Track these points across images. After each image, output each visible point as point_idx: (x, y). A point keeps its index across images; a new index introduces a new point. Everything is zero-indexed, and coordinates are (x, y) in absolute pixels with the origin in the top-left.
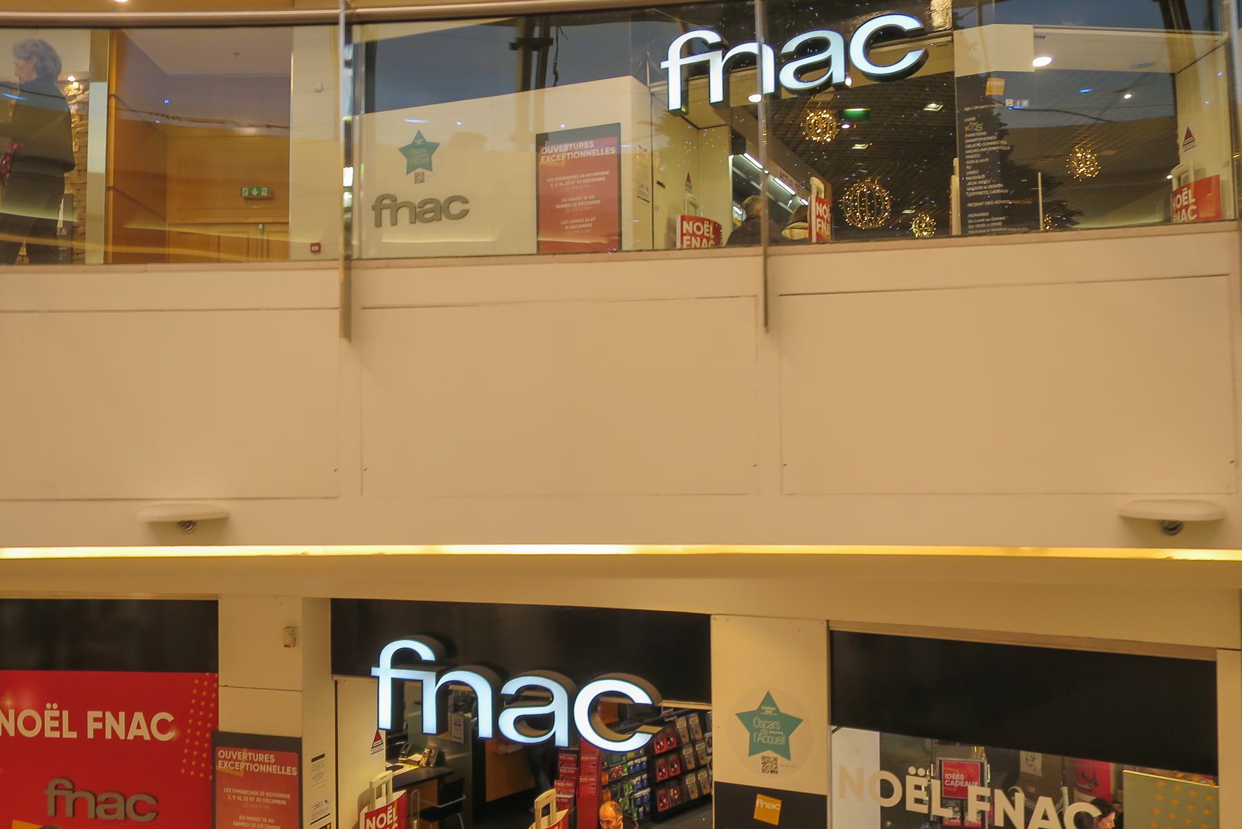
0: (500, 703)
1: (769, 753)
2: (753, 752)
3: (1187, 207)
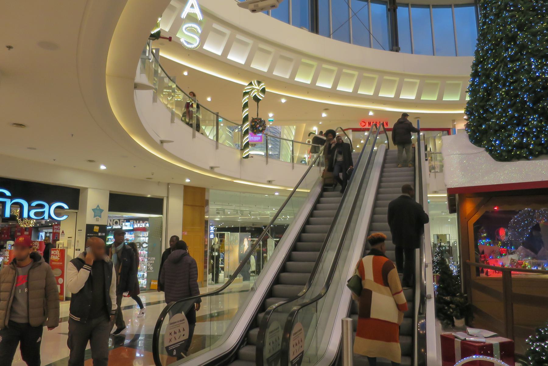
0: (30, 208)
1: (98, 217)
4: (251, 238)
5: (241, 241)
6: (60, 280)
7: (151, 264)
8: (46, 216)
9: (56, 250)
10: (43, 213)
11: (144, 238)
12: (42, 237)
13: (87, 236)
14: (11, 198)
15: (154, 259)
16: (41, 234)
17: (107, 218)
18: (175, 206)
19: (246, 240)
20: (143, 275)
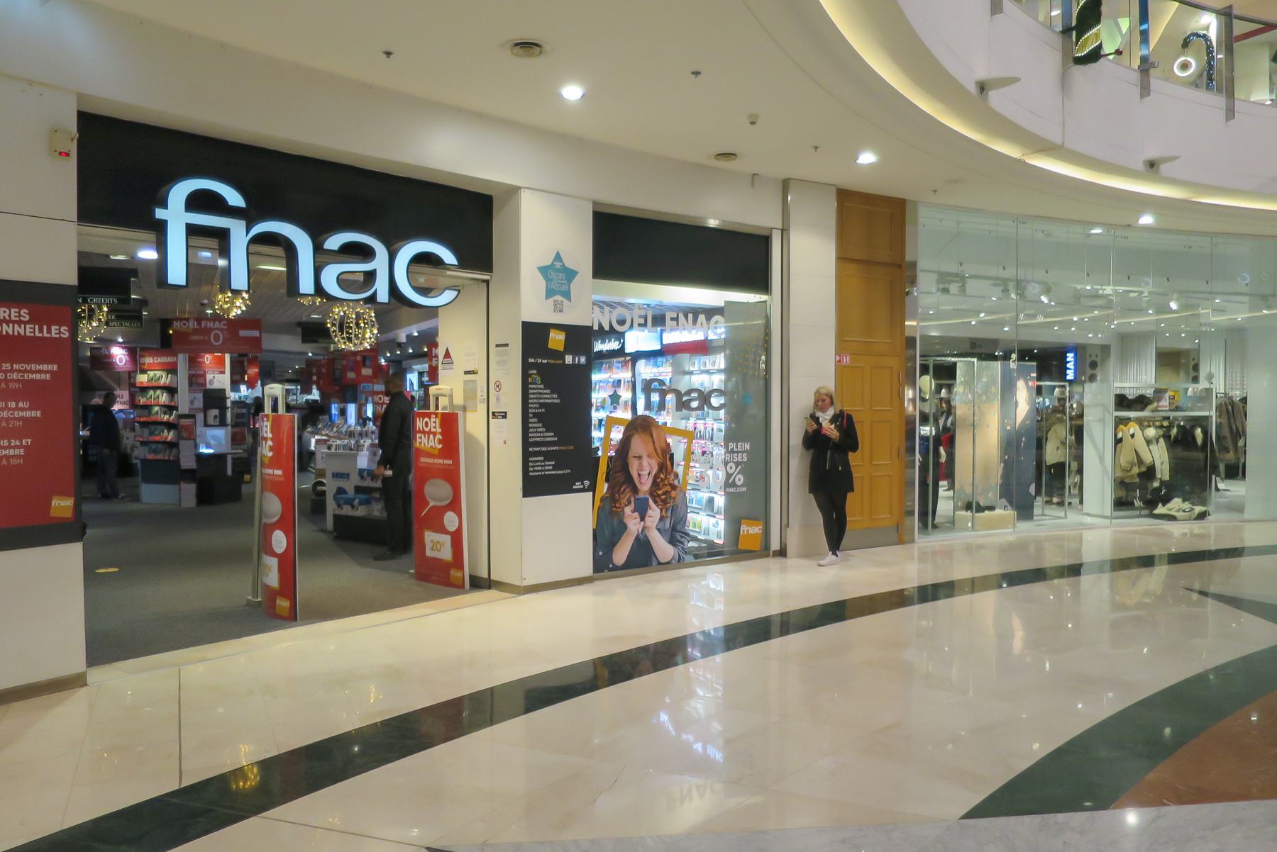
0: (322, 257)
1: (558, 298)
2: (547, 297)
3: (435, 434)
4: (1039, 378)
5: (1008, 389)
6: (450, 520)
7: (737, 464)
8: (381, 290)
9: (429, 415)
10: (370, 276)
11: (709, 374)
12: (412, 384)
13: (526, 367)
14: (249, 216)
15: (747, 446)
16: (409, 376)
17: (590, 301)
18: (810, 260)
19: (1021, 384)
20: (711, 501)
